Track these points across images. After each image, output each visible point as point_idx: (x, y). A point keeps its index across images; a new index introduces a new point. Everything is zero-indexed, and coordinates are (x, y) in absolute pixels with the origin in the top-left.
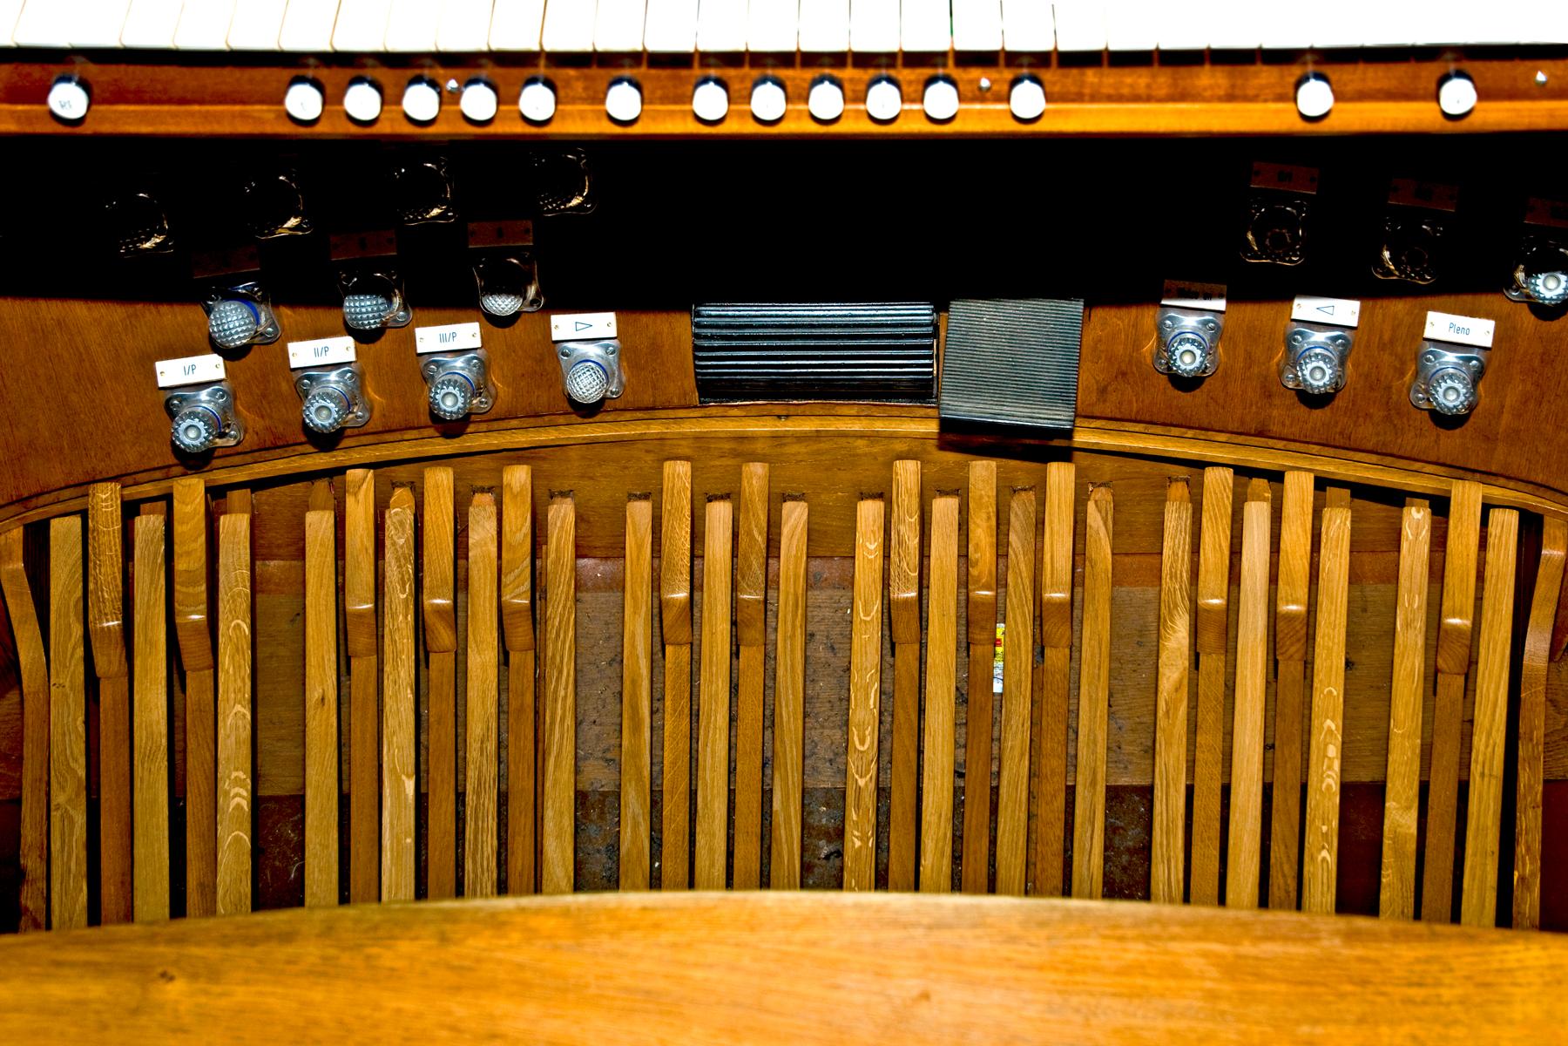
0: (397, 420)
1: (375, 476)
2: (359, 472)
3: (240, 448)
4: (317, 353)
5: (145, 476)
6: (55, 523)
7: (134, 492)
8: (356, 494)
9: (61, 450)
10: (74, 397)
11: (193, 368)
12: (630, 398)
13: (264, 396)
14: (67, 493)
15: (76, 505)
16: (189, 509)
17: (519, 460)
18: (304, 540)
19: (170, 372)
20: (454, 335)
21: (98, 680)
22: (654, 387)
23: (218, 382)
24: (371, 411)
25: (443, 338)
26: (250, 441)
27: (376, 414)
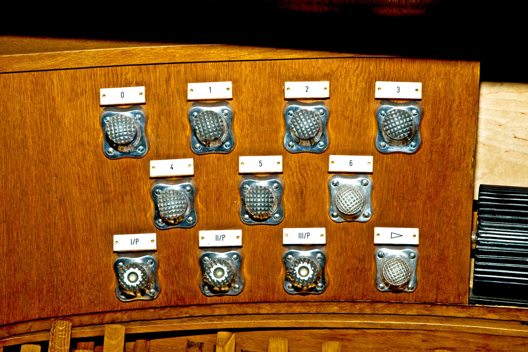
0: (260, 295)
1: (236, 338)
2: (225, 334)
3: (153, 303)
4: (217, 238)
5: (86, 319)
6: (23, 347)
7: (80, 333)
8: (223, 347)
9: (41, 291)
10: (58, 255)
11: (137, 240)
12: (420, 295)
13: (176, 268)
14: (37, 326)
15: (41, 337)
16: (114, 342)
17: (333, 338)
18: (300, 227)
19: (122, 242)
20: (308, 234)
21: (134, 340)
22: (438, 288)
23: (153, 251)
24: (244, 285)
25: (301, 236)
26: (160, 300)
27: (246, 289)
